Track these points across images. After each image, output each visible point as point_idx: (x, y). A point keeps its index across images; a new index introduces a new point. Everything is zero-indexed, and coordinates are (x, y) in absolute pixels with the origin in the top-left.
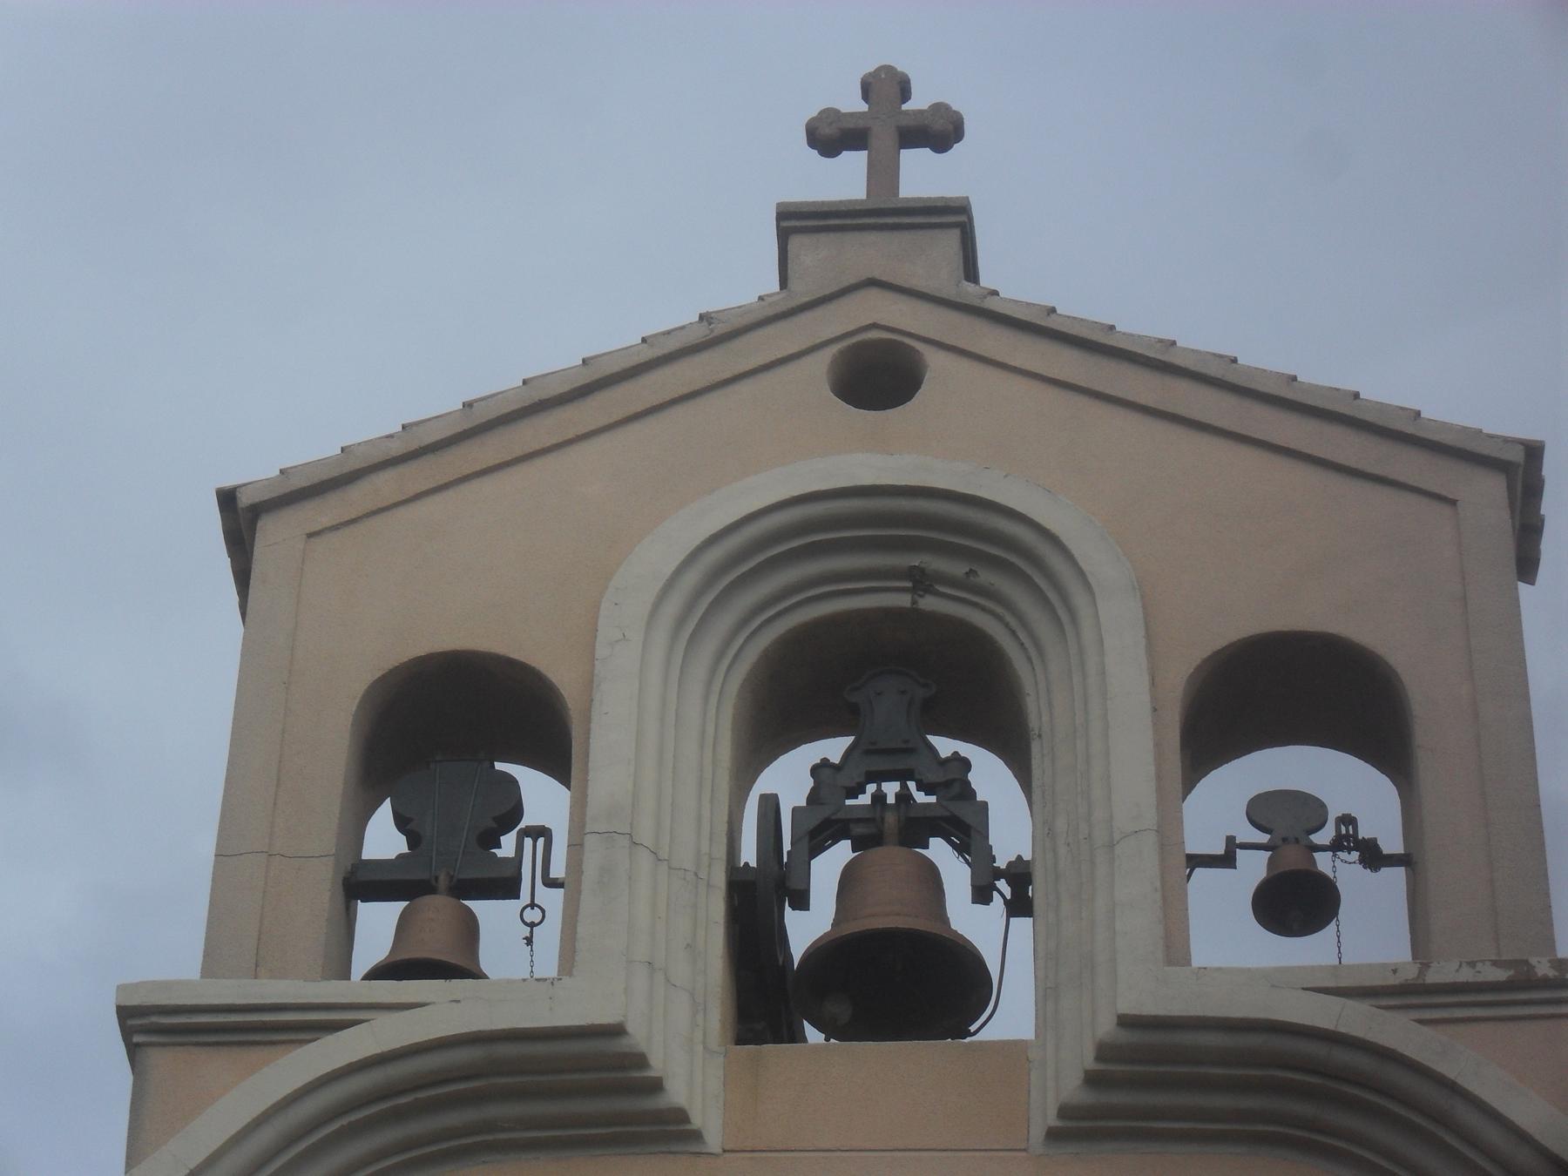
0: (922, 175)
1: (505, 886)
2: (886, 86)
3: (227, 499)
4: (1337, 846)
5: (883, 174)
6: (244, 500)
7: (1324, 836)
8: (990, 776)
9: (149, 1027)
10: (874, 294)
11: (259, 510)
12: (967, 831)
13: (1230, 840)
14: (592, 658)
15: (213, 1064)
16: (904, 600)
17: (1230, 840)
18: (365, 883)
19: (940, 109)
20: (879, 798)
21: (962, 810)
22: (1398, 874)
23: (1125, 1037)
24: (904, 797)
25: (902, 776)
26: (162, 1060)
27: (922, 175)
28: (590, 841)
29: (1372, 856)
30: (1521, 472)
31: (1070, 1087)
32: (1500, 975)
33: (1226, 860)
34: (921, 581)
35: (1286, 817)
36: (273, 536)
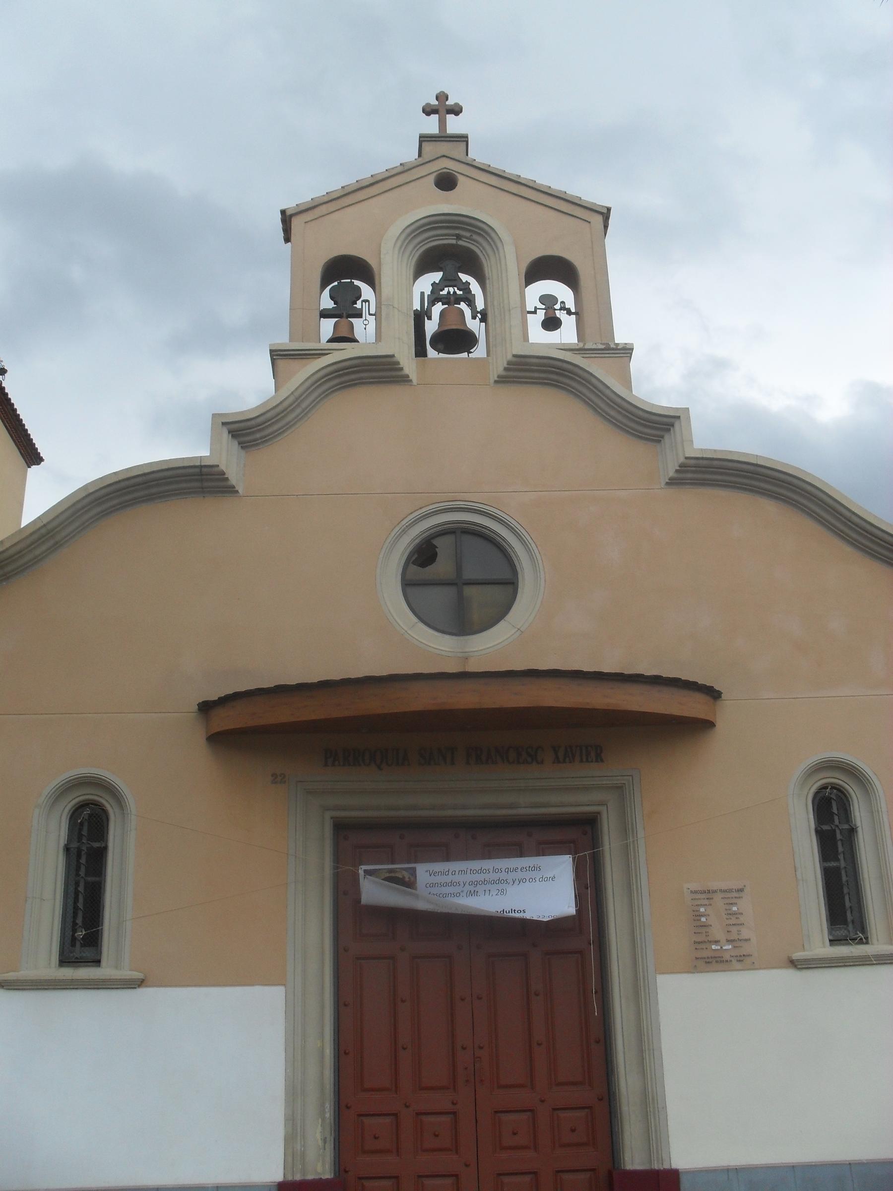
0: (454, 125)
1: (359, 315)
2: (442, 97)
3: (283, 212)
4: (560, 309)
5: (442, 124)
6: (288, 213)
7: (557, 306)
8: (475, 288)
9: (277, 355)
10: (444, 158)
11: (291, 216)
12: (471, 302)
13: (536, 308)
14: (380, 258)
15: (294, 364)
16: (454, 242)
17: (536, 308)
18: (325, 314)
19: (457, 104)
20: (449, 292)
21: (469, 296)
22: (574, 317)
23: (515, 359)
24: (455, 292)
25: (453, 286)
26: (281, 363)
27: (454, 125)
28: (383, 307)
29: (569, 312)
30: (605, 214)
31: (500, 370)
32: (603, 347)
33: (535, 312)
34: (459, 237)
35: (548, 301)
36: (296, 223)
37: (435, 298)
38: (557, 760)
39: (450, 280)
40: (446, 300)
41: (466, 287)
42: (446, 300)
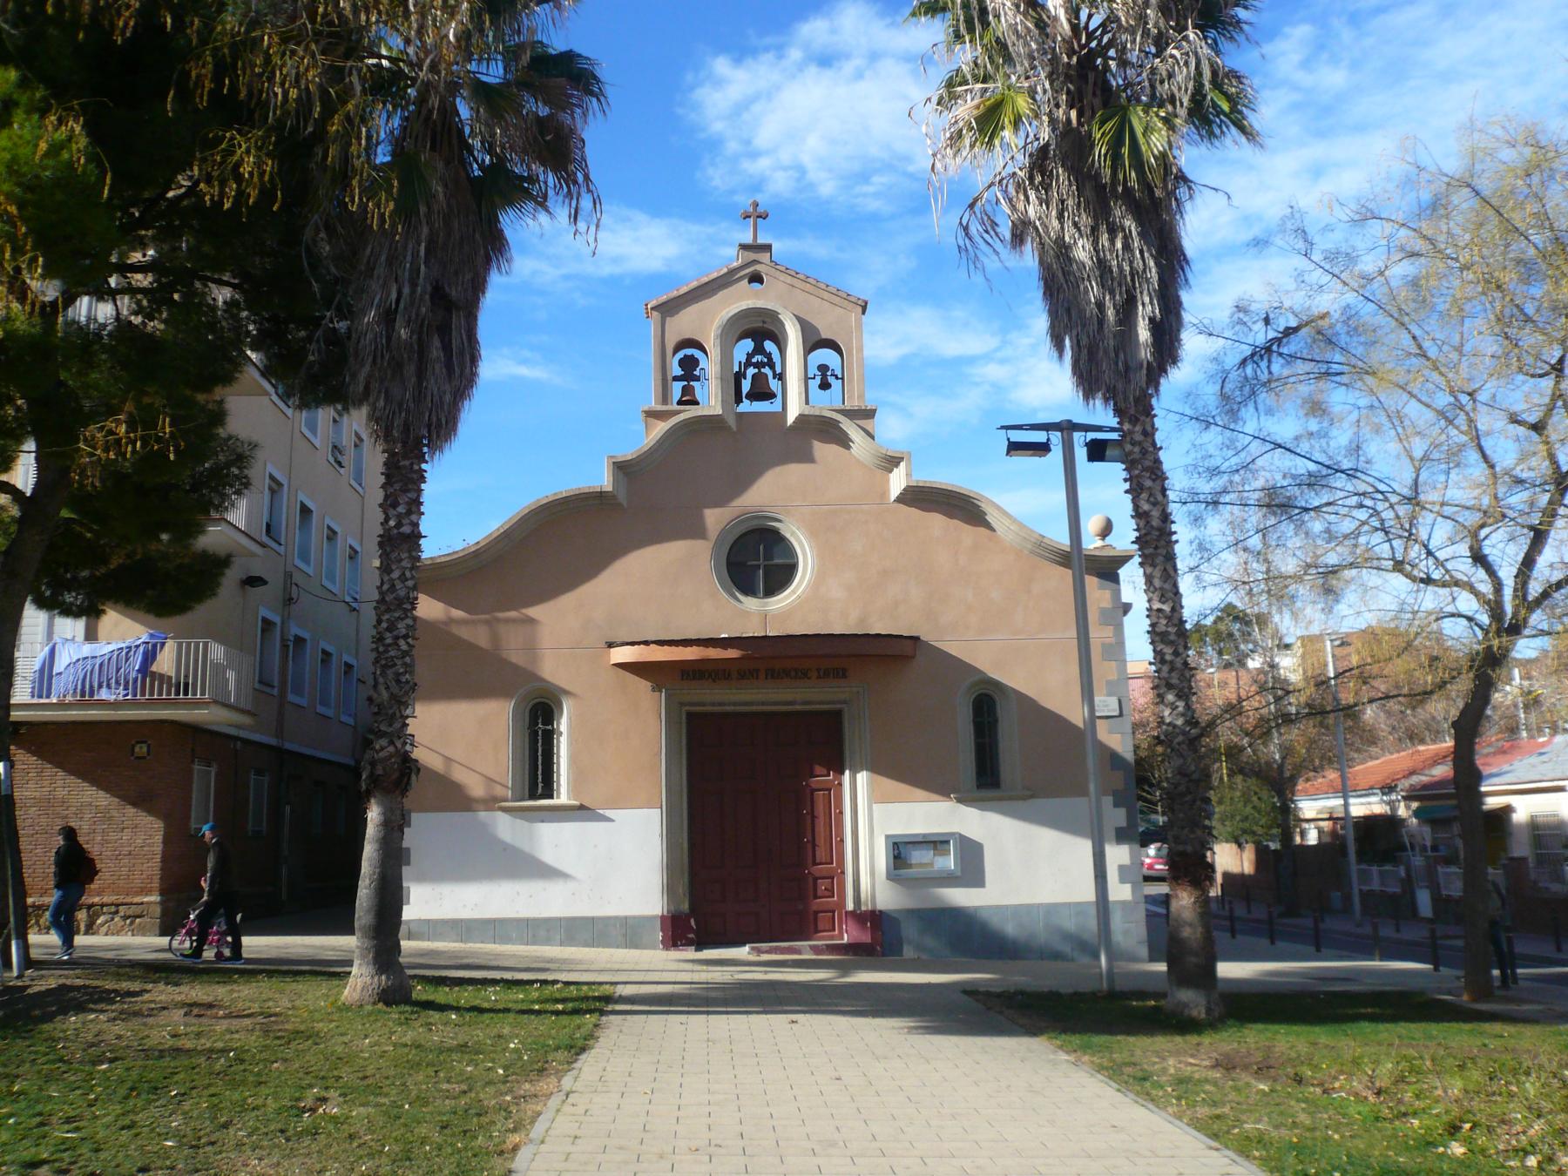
12: (772, 366)
18: (676, 379)
35: (823, 368)
37: (748, 363)
38: (819, 677)
39: (759, 349)
40: (756, 365)
41: (769, 356)
42: (756, 365)
